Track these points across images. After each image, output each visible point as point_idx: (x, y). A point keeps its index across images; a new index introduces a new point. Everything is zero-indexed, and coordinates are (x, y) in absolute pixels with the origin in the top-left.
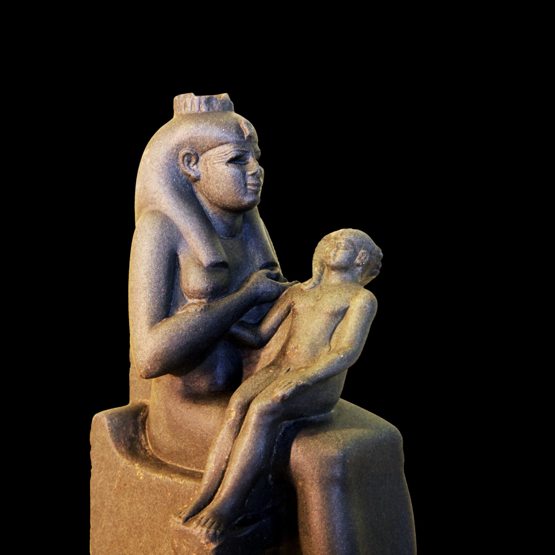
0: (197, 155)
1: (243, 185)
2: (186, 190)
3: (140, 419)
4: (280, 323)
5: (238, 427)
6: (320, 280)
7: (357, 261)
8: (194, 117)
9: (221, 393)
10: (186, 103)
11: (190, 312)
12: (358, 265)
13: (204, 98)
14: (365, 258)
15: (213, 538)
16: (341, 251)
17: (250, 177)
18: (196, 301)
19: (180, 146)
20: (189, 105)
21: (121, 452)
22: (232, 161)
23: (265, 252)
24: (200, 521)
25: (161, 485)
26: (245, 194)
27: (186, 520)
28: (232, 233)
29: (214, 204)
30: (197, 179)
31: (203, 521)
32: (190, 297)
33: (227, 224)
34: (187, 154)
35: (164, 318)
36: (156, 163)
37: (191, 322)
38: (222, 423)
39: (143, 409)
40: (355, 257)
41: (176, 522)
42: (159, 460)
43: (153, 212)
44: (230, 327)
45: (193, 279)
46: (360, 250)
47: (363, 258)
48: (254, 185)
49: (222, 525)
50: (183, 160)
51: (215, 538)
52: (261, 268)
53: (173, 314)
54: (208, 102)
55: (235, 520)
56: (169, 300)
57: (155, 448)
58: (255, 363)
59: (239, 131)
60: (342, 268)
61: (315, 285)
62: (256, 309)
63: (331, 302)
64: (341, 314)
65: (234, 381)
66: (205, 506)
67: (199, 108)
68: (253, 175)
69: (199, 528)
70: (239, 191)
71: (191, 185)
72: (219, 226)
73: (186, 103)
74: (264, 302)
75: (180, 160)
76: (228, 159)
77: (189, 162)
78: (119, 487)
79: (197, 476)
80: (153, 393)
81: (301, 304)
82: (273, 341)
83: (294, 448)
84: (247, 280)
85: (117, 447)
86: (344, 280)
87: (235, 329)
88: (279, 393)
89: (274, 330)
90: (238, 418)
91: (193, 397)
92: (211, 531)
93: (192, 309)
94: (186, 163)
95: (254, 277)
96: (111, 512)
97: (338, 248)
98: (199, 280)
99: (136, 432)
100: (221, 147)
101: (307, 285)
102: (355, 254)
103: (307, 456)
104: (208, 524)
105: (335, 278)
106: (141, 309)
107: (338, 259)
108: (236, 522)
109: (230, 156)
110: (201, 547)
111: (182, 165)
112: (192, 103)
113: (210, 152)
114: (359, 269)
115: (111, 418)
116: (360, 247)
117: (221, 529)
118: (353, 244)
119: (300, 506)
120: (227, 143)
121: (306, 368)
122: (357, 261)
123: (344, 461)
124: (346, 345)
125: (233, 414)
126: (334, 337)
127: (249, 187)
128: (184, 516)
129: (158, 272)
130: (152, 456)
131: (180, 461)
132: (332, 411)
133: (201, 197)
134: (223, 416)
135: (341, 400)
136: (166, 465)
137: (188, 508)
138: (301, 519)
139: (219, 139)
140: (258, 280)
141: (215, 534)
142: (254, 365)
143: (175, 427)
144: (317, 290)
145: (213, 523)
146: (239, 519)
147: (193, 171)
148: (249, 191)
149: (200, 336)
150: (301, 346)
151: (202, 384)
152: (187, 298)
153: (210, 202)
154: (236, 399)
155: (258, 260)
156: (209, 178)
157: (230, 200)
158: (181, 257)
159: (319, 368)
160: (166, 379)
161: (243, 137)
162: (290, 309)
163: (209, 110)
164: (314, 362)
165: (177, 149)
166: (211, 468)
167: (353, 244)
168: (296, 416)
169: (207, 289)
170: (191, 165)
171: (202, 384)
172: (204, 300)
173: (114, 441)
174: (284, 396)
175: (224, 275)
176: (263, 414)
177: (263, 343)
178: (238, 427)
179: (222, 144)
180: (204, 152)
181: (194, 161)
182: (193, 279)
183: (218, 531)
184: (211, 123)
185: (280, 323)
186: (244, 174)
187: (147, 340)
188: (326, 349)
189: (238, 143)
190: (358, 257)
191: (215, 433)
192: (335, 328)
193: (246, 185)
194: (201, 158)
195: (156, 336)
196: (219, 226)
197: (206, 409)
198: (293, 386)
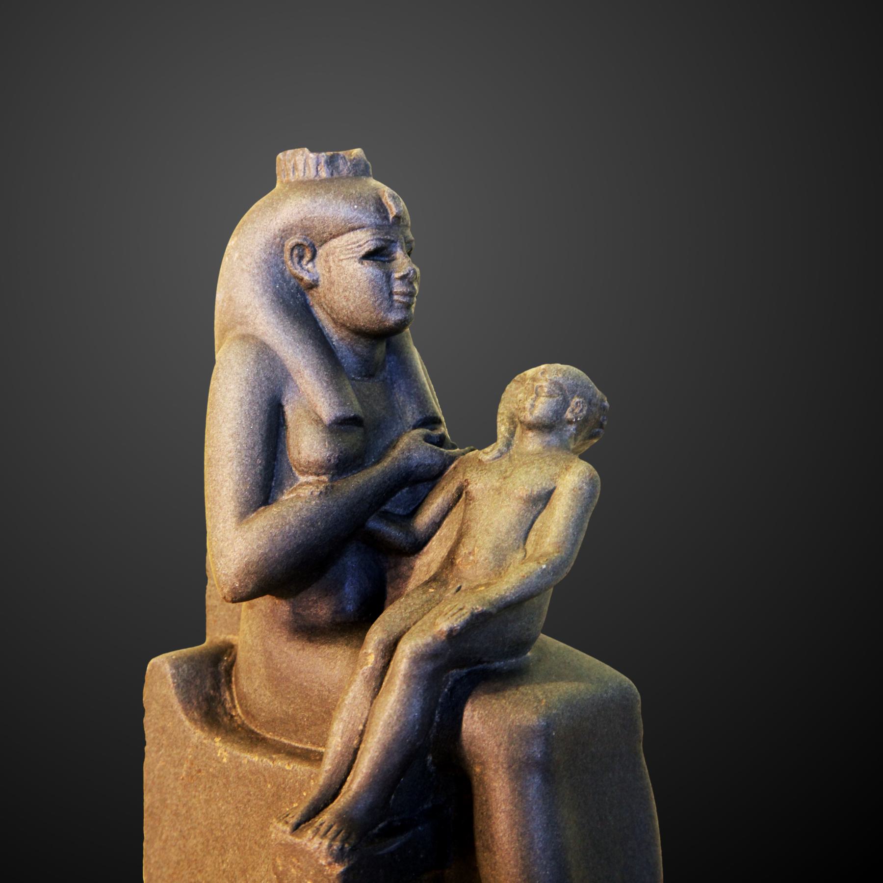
0: (313, 246)
1: (386, 295)
2: (296, 302)
3: (222, 667)
4: (445, 513)
5: (379, 680)
6: (509, 445)
7: (569, 415)
8: (309, 186)
9: (352, 626)
10: (298, 163)
11: (303, 496)
12: (570, 422)
13: (324, 156)
14: (581, 411)
15: (339, 856)
16: (542, 399)
17: (398, 282)
18: (311, 478)
19: (286, 233)
20: (301, 167)
21: (192, 720)
22: (369, 256)
23: (422, 400)
24: (318, 829)
25: (256, 771)
26: (391, 308)
27: (297, 828)
28: (369, 370)
29: (340, 324)
30: (313, 285)
31: (323, 829)
32: (303, 473)
33: (368, 356)
34: (298, 245)
35: (261, 506)
36: (248, 260)
37: (304, 513)
38: (354, 673)
39: (226, 651)
40: (565, 410)
41: (280, 831)
42: (253, 732)
43: (244, 338)
44: (366, 521)
45: (307, 444)
46: (573, 398)
47: (577, 411)
48: (404, 294)
49: (353, 836)
50: (291, 255)
51: (342, 855)
52: (415, 427)
53: (275, 500)
54: (331, 162)
55: (374, 828)
56: (268, 477)
57: (247, 713)
58: (406, 578)
59: (381, 208)
60: (544, 427)
61: (501, 454)
62: (407, 492)
63: (526, 481)
64: (542, 500)
65: (372, 607)
66: (326, 805)
67: (317, 171)
68: (403, 278)
69: (317, 840)
70: (381, 304)
71: (303, 295)
72: (348, 359)
73: (298, 163)
74: (420, 481)
75: (287, 255)
76: (363, 253)
77: (301, 258)
78: (189, 774)
79: (313, 758)
80: (244, 626)
81: (479, 484)
82: (434, 542)
83: (467, 713)
84: (392, 445)
85: (186, 711)
86: (548, 446)
87: (373, 524)
88: (444, 625)
89: (436, 525)
90: (379, 666)
91: (308, 631)
92: (336, 845)
93: (305, 492)
94: (296, 260)
95: (405, 441)
96: (176, 814)
97: (538, 395)
98: (317, 446)
99: (216, 687)
100: (352, 234)
101: (488, 454)
102: (565, 403)
103: (488, 726)
104: (330, 834)
105: (532, 443)
106: (224, 492)
107: (537, 412)
108: (376, 831)
109: (366, 248)
110: (320, 870)
111: (289, 263)
112: (306, 164)
113: (335, 242)
114: (572, 428)
115: (176, 665)
116: (573, 393)
117: (352, 842)
118: (561, 389)
119: (477, 805)
120: (361, 227)
121: (488, 585)
122: (569, 415)
123: (547, 734)
124: (551, 550)
125: (371, 659)
126: (532, 537)
127: (396, 297)
128: (293, 821)
129: (251, 433)
130: (242, 726)
131: (286, 733)
132: (529, 654)
133: (320, 314)
134: (355, 661)
135: (542, 636)
136: (264, 740)
137: (298, 808)
138: (479, 826)
139: (349, 221)
140: (410, 446)
141: (342, 849)
142: (405, 581)
143: (278, 680)
144: (505, 461)
145: (338, 833)
146: (380, 826)
147: (306, 272)
148: (396, 304)
149: (319, 535)
150: (479, 551)
151: (322, 610)
152: (297, 473)
153: (335, 321)
154: (376, 635)
155: (411, 414)
156: (332, 283)
157: (365, 317)
158: (288, 410)
159: (507, 585)
160: (264, 602)
161: (387, 218)
162: (461, 492)
163: (332, 174)
164: (499, 575)
165: (282, 238)
166: (335, 744)
167: (561, 389)
168: (475, 661)
169: (330, 461)
170: (304, 262)
171: (322, 610)
172: (324, 478)
173: (181, 701)
174: (451, 631)
175: (357, 438)
176: (419, 659)
177: (418, 545)
178: (379, 680)
179: (353, 229)
180: (324, 242)
181: (308, 256)
182: (307, 444)
183: (346, 845)
184: (336, 196)
185: (445, 513)
186: (388, 276)
187: (234, 542)
188: (519, 556)
189: (379, 227)
190: (570, 409)
191: (342, 689)
192: (533, 522)
193: (391, 294)
194: (320, 252)
195: (249, 535)
196: (348, 359)
197: (328, 650)
198: (466, 615)
